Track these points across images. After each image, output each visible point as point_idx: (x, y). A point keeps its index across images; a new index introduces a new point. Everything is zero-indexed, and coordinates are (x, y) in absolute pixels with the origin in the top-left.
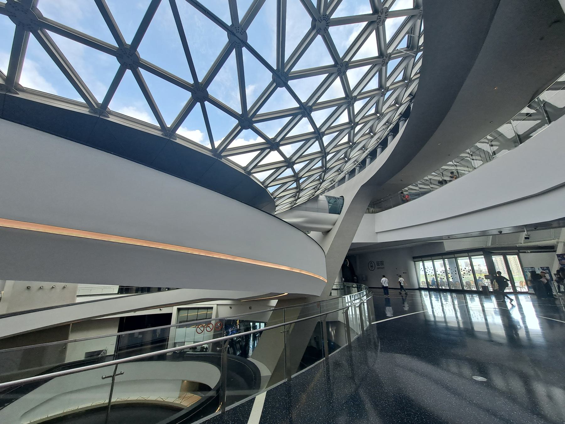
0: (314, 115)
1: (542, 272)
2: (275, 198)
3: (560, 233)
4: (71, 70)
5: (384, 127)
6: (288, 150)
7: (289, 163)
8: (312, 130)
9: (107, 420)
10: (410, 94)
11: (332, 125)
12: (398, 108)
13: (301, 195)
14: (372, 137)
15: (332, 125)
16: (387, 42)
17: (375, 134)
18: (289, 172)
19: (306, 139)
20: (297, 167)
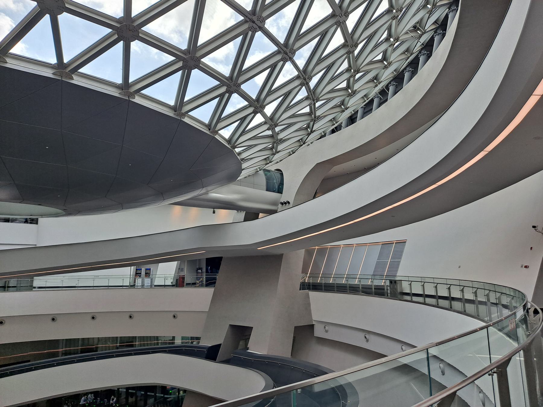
0: (270, 24)
1: (182, 343)
2: (242, 159)
3: (353, 382)
4: (83, 9)
5: (404, 56)
6: (253, 87)
7: (256, 105)
8: (275, 48)
9: (430, 14)
10: (436, 22)
11: (273, 88)
12: (420, 36)
13: (280, 148)
14: (386, 67)
15: (273, 88)
16: (266, 3)
17: (390, 64)
18: (259, 119)
19: (272, 65)
20: (269, 110)
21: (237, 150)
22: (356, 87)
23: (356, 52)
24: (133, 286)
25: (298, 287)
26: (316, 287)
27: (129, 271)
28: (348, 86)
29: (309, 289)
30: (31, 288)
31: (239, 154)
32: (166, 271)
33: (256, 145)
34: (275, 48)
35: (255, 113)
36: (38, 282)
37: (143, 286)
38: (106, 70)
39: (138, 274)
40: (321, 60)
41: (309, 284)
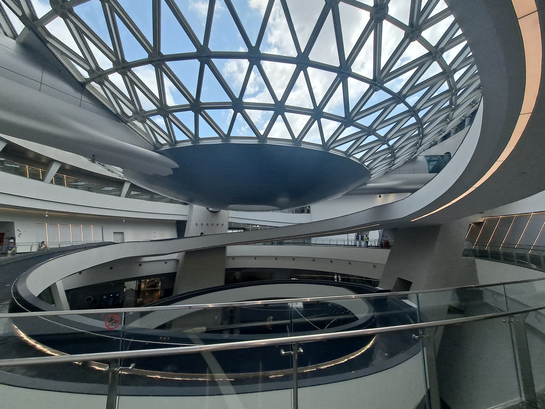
8: (368, 86)
21: (366, 164)
22: (459, 102)
23: (458, 94)
24: (355, 246)
25: (446, 311)
26: (483, 255)
27: (353, 236)
28: (451, 104)
29: (476, 256)
30: (310, 244)
31: (368, 166)
32: (374, 236)
33: (379, 157)
34: (368, 86)
35: (90, 72)
36: (314, 240)
37: (360, 246)
38: (313, 138)
39: (357, 238)
40: (430, 100)
41: (474, 251)
